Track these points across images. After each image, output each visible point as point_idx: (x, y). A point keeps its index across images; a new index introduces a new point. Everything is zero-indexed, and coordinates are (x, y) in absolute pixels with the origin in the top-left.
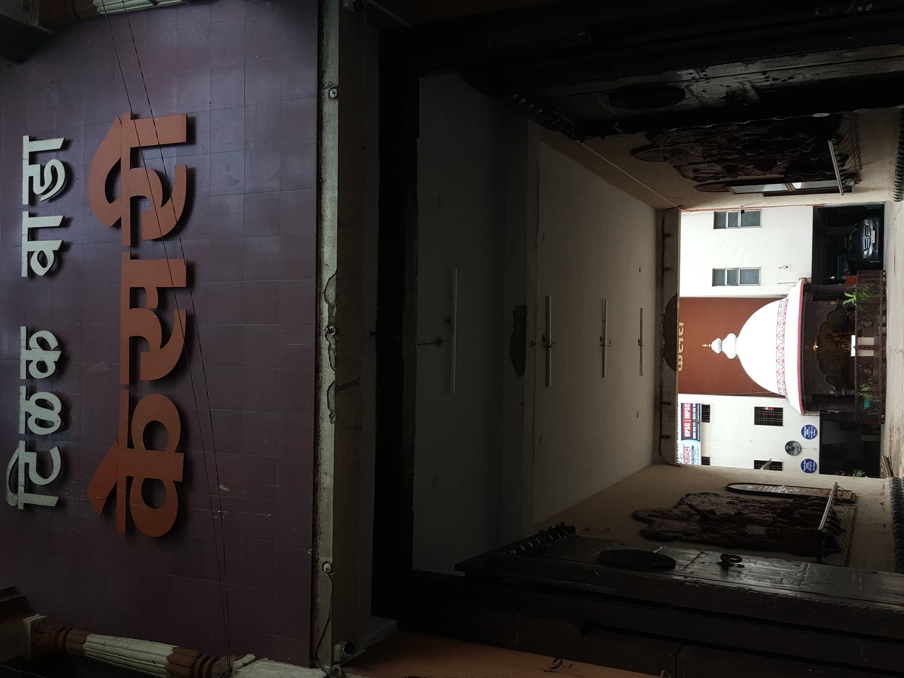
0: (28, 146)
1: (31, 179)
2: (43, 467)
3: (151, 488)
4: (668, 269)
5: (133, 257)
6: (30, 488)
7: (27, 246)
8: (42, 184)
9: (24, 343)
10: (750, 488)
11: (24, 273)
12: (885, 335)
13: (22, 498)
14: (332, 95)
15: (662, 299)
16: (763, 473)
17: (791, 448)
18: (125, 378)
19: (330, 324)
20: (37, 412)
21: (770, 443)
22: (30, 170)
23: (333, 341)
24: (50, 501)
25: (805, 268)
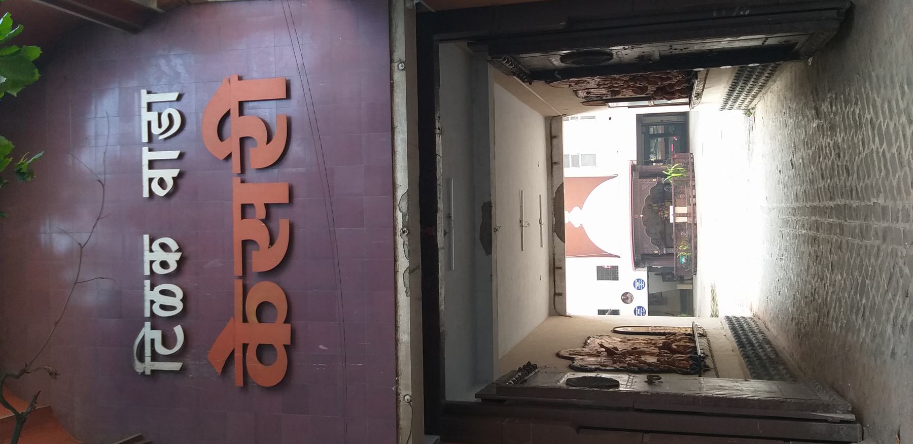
0: (146, 98)
1: (149, 123)
2: (167, 341)
3: (262, 350)
4: (556, 163)
5: (243, 182)
6: (155, 356)
7: (147, 174)
8: (160, 126)
9: (147, 247)
10: (630, 330)
11: (146, 194)
12: (695, 204)
13: (148, 366)
14: (401, 68)
15: (552, 186)
16: (607, 317)
17: (626, 298)
18: (238, 271)
19: (403, 227)
20: (161, 300)
21: (608, 294)
22: (146, 116)
23: (406, 239)
24: (176, 366)
25: (631, 154)
